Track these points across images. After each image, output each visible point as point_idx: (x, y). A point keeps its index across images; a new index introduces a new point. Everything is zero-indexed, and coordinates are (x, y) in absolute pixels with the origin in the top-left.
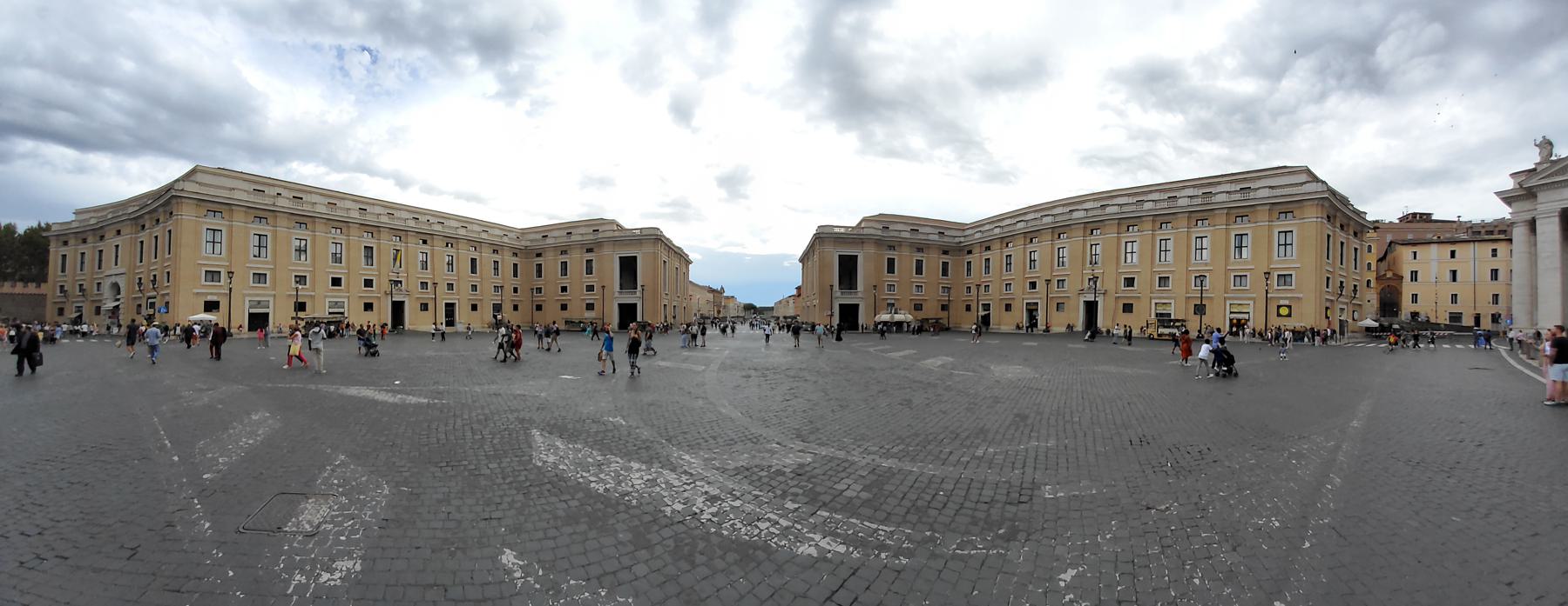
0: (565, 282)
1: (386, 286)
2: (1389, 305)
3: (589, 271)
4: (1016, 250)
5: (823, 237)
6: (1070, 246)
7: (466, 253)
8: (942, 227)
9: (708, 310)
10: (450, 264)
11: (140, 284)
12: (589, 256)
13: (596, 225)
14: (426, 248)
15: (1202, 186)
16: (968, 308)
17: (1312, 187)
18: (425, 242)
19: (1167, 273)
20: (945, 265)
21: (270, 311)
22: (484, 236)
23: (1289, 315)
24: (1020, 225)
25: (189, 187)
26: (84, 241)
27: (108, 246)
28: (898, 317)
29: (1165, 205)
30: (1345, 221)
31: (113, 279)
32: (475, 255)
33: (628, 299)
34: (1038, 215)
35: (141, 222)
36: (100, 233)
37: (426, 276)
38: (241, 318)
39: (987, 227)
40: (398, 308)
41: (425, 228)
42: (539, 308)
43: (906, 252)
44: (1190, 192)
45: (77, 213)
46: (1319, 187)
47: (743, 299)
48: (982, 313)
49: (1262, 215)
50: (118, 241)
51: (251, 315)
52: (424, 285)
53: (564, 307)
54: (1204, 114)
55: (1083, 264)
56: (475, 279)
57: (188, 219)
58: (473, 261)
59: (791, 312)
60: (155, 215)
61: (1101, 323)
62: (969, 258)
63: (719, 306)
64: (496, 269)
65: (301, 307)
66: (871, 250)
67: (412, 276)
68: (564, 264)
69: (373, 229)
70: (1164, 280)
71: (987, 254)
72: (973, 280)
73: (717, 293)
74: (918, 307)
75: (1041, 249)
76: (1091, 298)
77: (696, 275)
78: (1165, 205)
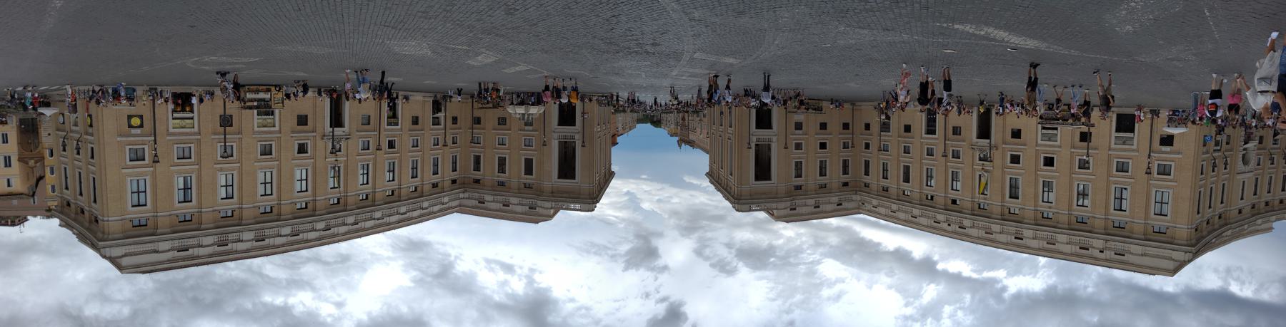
0: (822, 154)
1: (996, 155)
2: (29, 130)
3: (798, 166)
4: (409, 184)
5: (589, 199)
6: (357, 186)
7: (912, 188)
8: (480, 209)
9: (693, 120)
10: (929, 177)
11: (1226, 164)
12: (799, 182)
14: (953, 195)
15: (228, 253)
16: (455, 120)
17: (116, 252)
18: (954, 202)
19: (270, 158)
20: (477, 168)
21: (1114, 134)
22: (894, 207)
23: (130, 117)
24: (403, 209)
25: (1179, 256)
26: (1267, 204)
27: (1250, 198)
29: (268, 232)
30: (80, 217)
31: (1247, 168)
32: (904, 186)
33: (764, 133)
34: (386, 220)
35: (1222, 222)
36: (1255, 211)
37: (953, 164)
38: (1141, 128)
39: (436, 208)
40: (984, 132)
41: (953, 217)
42: (846, 126)
43: (514, 183)
44: (241, 246)
45: (1271, 229)
46: (108, 252)
47: (661, 132)
48: (441, 115)
49: (164, 222)
50: (1241, 204)
51: (1132, 131)
52: (956, 155)
53: (823, 126)
55: (346, 167)
56: (906, 159)
57: (1181, 222)
58: (907, 180)
59: (620, 117)
60: (1210, 228)
61: (326, 102)
62: (454, 175)
63: (683, 125)
64: (885, 170)
65: (1085, 137)
67: (968, 164)
68: (823, 173)
69: (1009, 217)
70: (267, 151)
71: (436, 179)
73: (685, 141)
74: (502, 121)
75: (384, 184)
76: (338, 131)
77: (702, 160)
78: (268, 232)
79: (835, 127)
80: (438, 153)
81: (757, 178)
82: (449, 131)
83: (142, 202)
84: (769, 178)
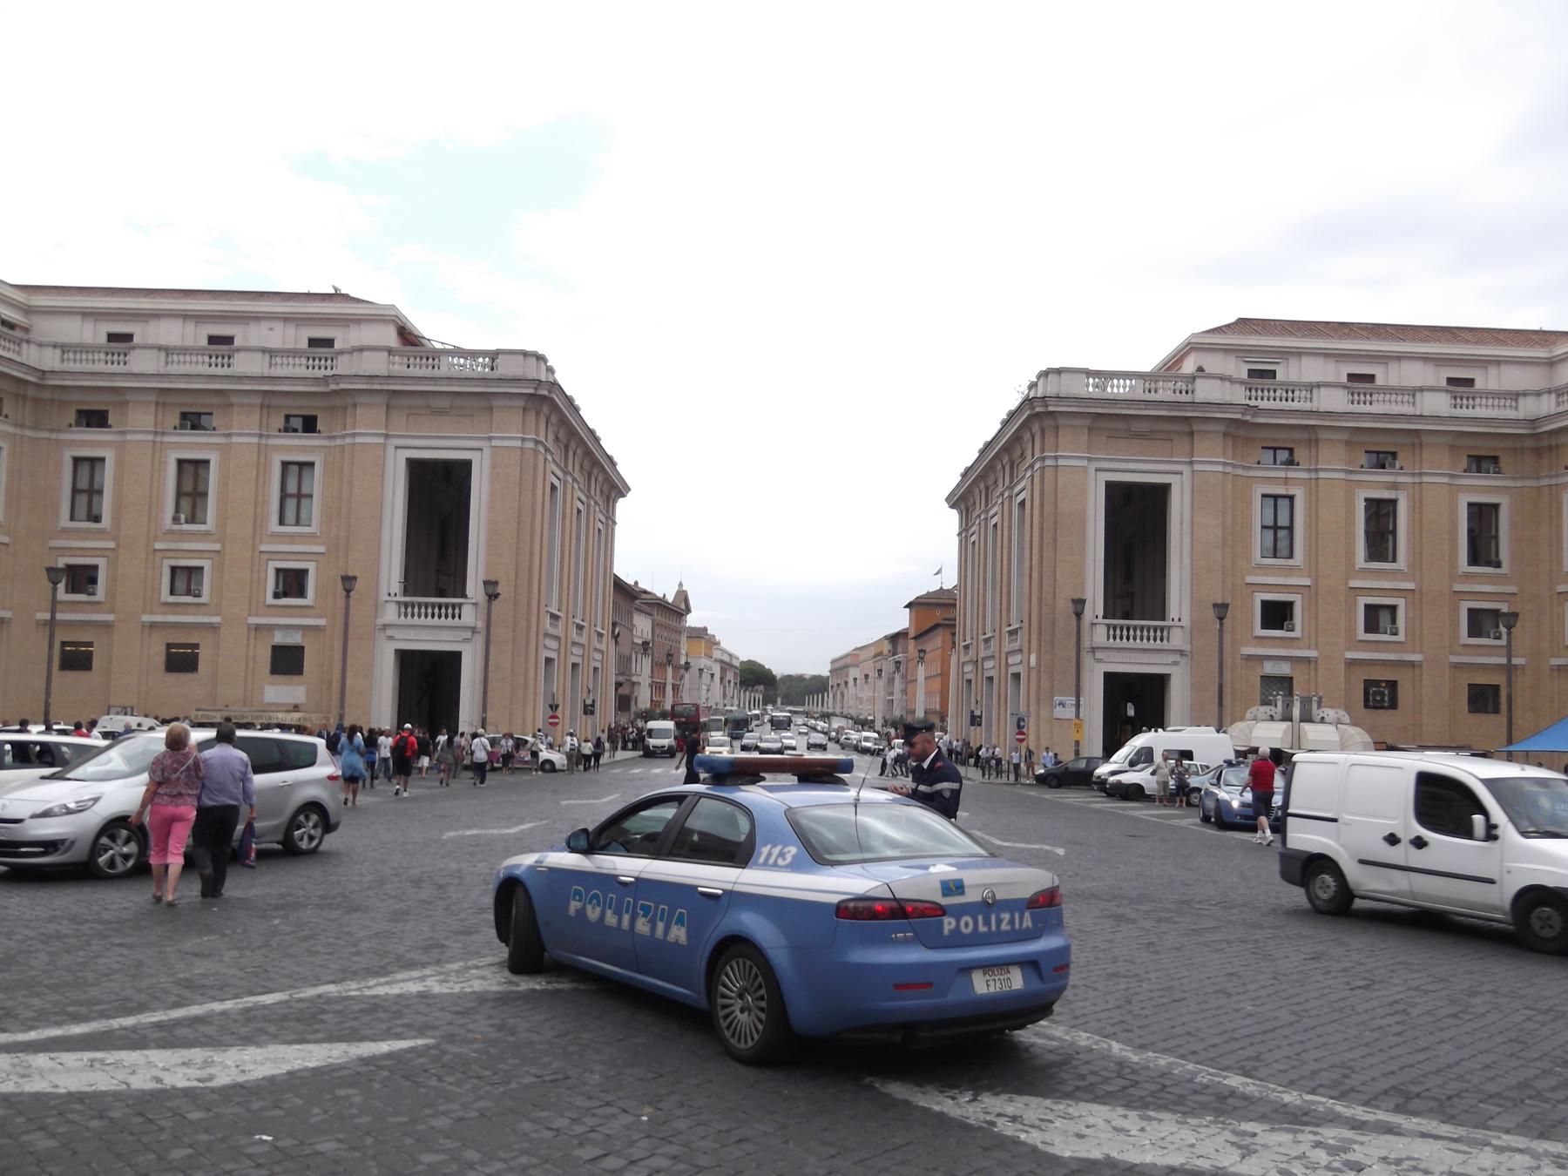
0: (194, 548)
5: (1046, 418)
13: (323, 319)
33: (430, 637)
43: (1333, 465)
66: (1212, 460)
68: (192, 469)
81: (1160, 493)
83: (84, 471)
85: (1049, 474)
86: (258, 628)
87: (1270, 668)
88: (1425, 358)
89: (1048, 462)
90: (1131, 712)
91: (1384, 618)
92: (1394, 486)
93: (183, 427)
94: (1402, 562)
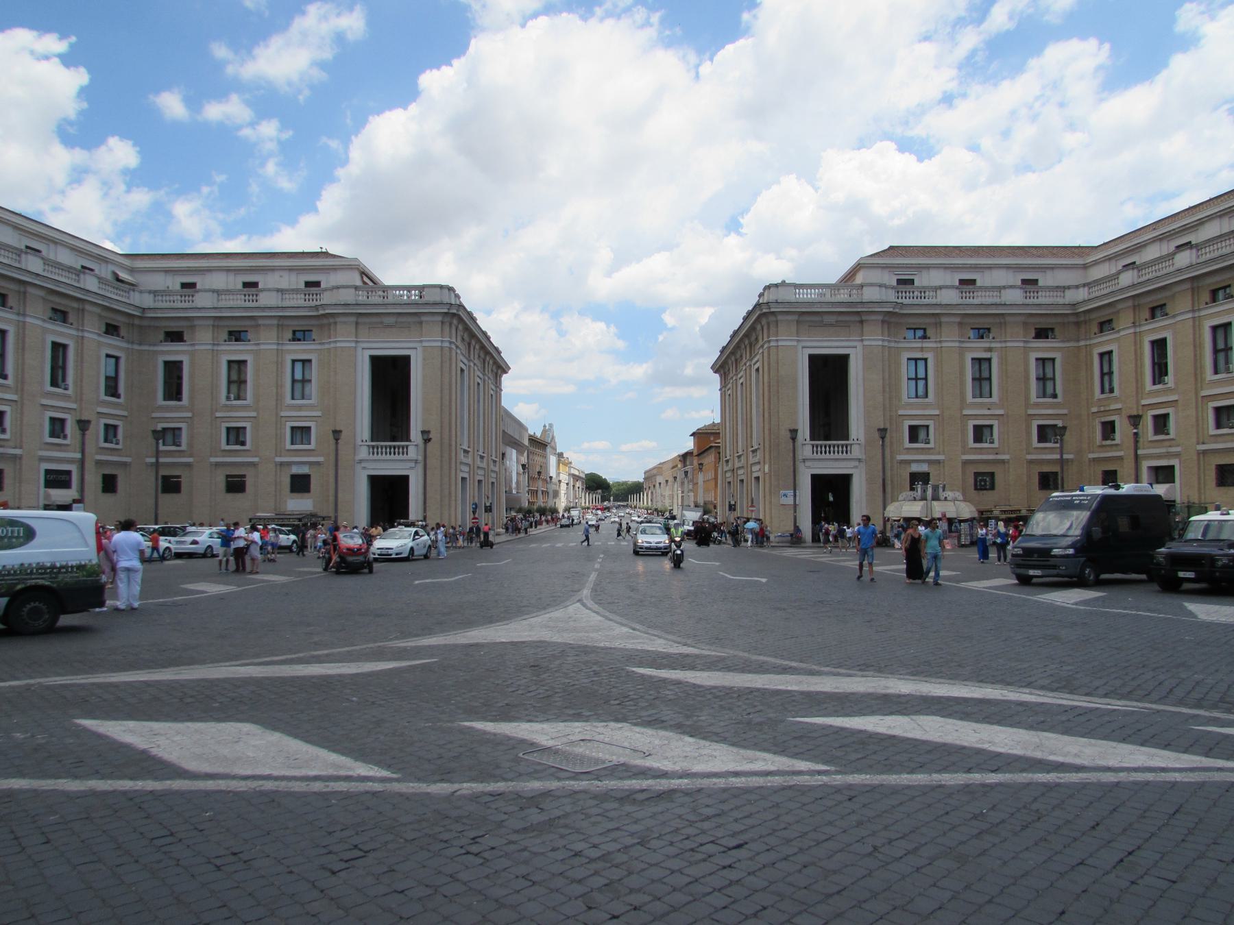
0: (240, 415)
5: (768, 317)
8: (1030, 263)
22: (33, 264)
28: (938, 509)
33: (389, 466)
39: (1152, 253)
43: (949, 339)
54: (1226, 107)
62: (1105, 342)
66: (875, 338)
68: (238, 366)
72: (1120, 404)
79: (204, 485)
80: (1153, 396)
81: (843, 360)
82: (1126, 452)
83: (299, 366)
84: (376, 362)
85: (773, 351)
86: (282, 464)
87: (915, 468)
88: (1008, 267)
89: (772, 344)
90: (831, 499)
91: (922, 435)
92: (990, 350)
93: (230, 340)
94: (995, 398)
